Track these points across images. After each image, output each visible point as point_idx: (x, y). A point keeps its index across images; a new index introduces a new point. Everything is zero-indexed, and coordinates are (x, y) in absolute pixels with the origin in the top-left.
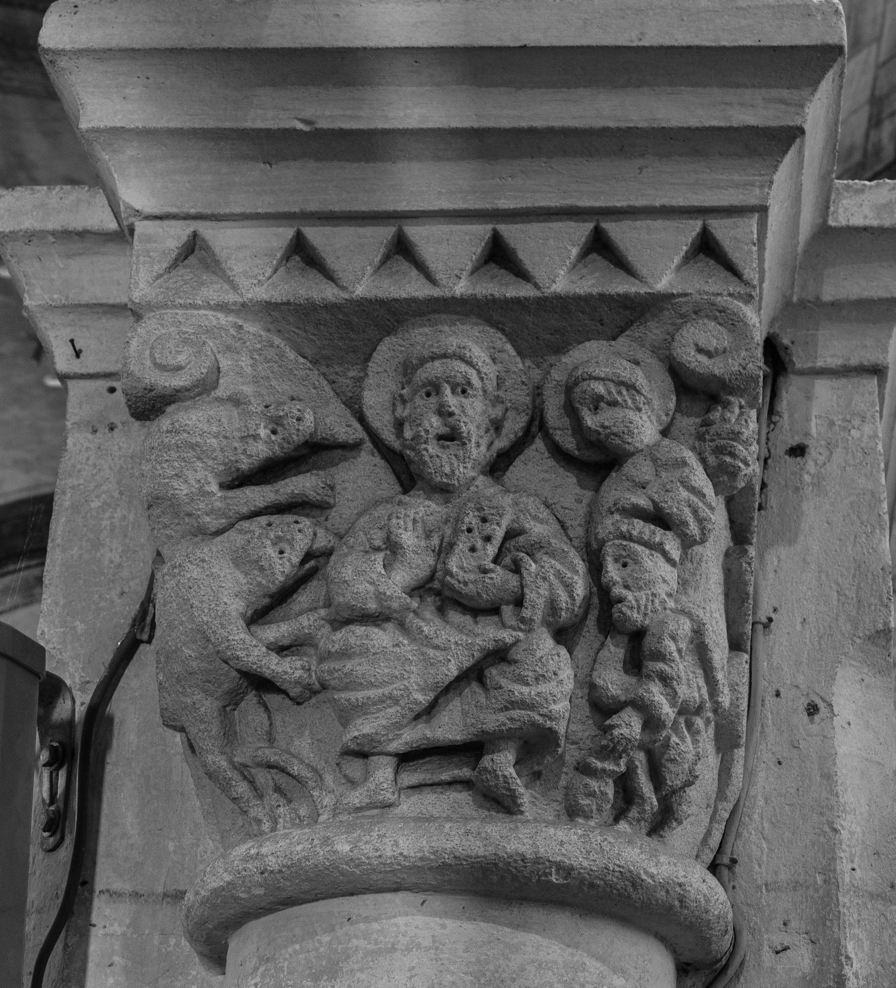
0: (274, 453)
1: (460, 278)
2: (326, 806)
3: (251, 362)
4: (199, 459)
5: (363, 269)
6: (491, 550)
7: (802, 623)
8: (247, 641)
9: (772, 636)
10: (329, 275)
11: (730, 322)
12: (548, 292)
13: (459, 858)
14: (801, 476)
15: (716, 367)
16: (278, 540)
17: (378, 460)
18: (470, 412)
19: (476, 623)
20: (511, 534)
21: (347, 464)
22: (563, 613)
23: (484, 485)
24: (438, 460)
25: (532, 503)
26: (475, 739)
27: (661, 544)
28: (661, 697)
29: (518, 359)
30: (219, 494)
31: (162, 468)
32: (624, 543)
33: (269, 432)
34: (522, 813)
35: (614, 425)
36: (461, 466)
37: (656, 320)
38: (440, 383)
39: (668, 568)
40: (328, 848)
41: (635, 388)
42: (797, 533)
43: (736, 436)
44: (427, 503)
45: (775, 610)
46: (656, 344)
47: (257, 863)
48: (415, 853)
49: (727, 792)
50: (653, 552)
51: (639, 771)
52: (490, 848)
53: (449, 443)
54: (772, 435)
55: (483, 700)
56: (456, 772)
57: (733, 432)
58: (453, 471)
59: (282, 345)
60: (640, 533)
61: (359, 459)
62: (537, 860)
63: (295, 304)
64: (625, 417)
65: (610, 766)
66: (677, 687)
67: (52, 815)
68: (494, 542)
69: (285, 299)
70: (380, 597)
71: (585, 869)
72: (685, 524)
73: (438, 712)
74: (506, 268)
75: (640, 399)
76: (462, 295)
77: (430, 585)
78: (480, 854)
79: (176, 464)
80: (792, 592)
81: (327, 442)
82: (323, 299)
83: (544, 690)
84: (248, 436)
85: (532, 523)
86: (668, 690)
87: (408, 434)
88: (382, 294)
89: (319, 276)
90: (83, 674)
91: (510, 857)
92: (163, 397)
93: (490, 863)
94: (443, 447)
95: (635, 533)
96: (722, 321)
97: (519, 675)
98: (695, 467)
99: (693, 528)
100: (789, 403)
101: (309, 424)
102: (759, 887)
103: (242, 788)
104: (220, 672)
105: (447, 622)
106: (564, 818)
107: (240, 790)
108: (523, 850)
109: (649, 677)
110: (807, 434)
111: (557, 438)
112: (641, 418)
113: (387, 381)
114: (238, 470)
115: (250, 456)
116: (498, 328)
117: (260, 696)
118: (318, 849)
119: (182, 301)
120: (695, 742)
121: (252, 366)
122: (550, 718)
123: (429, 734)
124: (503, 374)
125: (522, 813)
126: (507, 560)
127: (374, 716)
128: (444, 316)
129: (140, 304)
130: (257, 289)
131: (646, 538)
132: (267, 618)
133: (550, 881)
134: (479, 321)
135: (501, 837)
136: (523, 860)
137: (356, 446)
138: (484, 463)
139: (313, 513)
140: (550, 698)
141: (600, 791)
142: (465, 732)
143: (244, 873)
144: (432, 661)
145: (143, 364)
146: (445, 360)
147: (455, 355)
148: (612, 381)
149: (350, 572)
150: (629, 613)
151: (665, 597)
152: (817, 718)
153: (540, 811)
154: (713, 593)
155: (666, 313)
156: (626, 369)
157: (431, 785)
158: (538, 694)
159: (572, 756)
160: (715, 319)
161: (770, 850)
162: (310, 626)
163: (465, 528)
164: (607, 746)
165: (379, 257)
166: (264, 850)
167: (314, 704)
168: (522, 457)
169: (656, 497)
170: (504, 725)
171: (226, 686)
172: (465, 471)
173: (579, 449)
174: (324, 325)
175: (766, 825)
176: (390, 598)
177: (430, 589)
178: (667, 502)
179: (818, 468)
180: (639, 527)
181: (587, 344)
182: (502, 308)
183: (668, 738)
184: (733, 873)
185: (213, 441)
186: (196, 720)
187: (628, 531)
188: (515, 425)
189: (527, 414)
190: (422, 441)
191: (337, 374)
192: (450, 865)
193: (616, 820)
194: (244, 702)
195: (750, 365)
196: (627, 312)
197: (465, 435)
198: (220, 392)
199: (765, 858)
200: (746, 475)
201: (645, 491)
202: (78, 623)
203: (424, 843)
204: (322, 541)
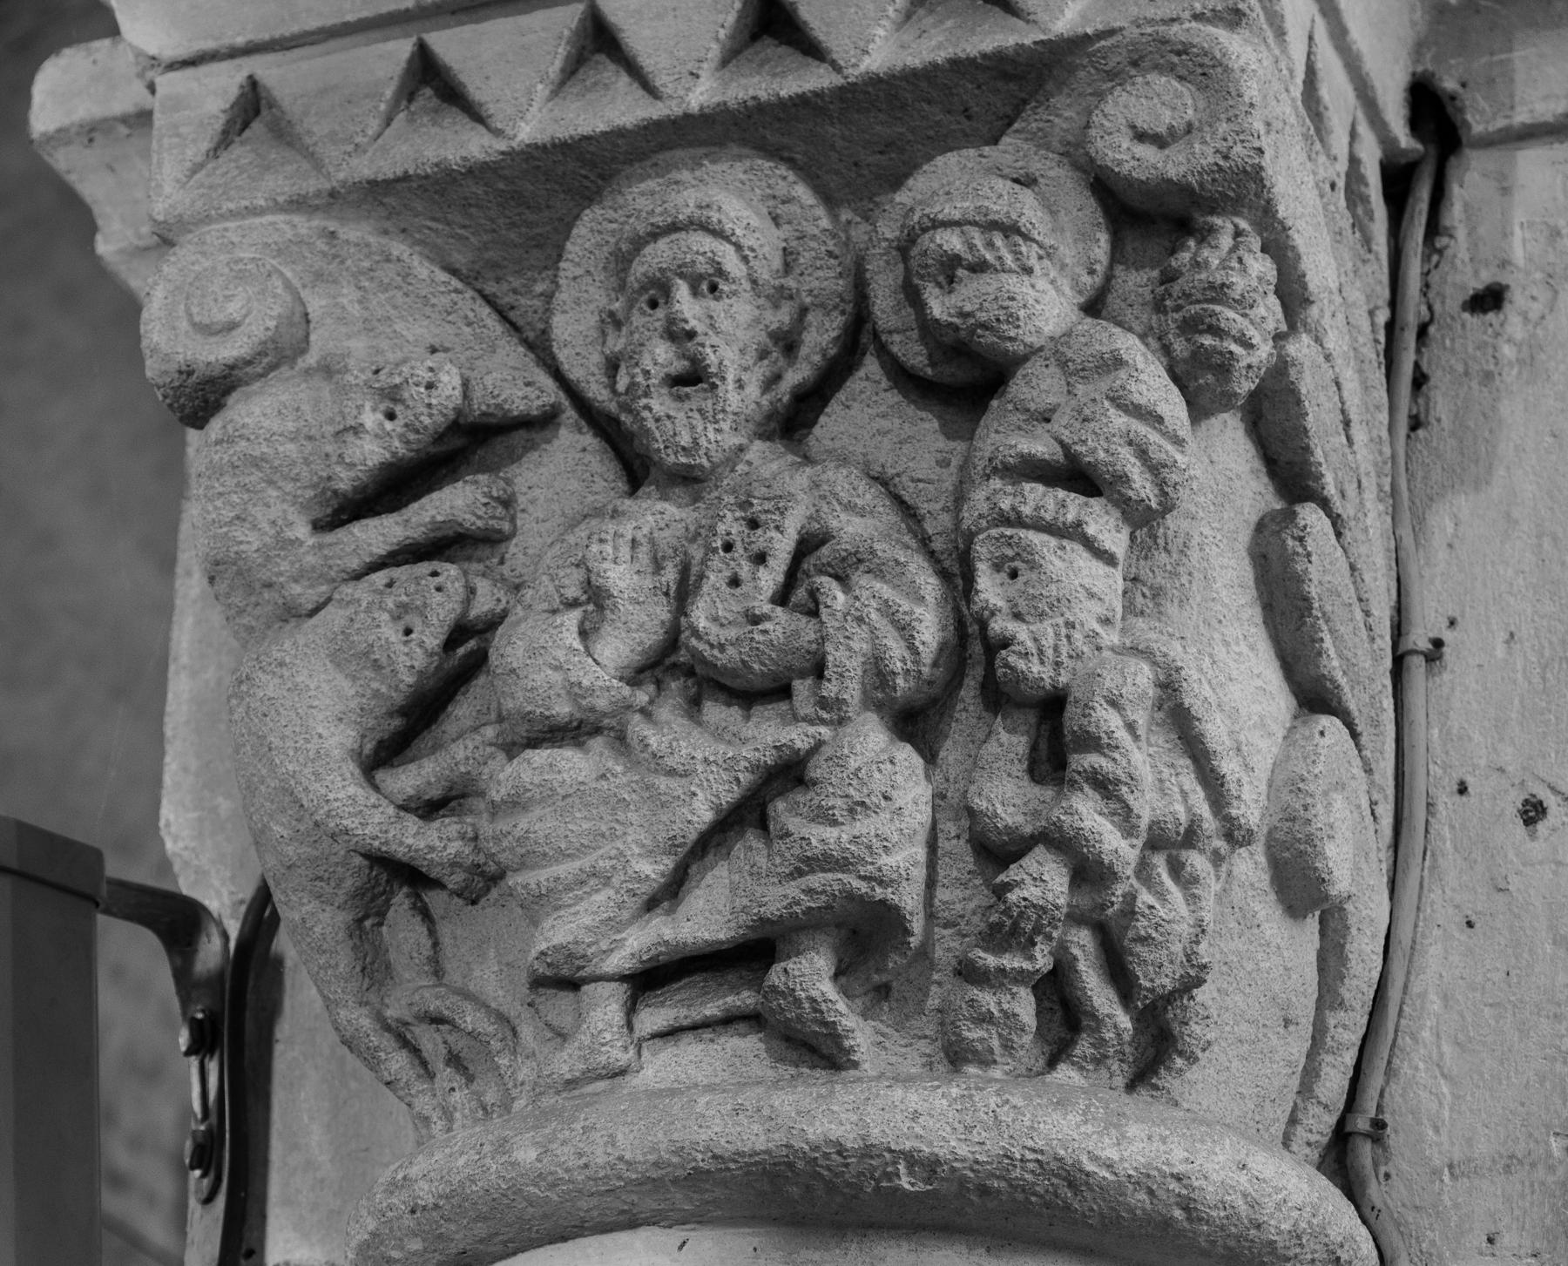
0: (394, 454)
1: (698, 77)
2: (522, 1084)
3: (360, 294)
4: (271, 482)
5: (529, 92)
6: (770, 578)
7: (1507, 642)
8: (361, 800)
9: (1446, 676)
10: (476, 115)
11: (1200, 71)
12: (853, 74)
13: (721, 1157)
14: (1495, 348)
15: (1173, 164)
16: (404, 608)
17: (589, 439)
18: (725, 324)
19: (747, 718)
20: (807, 545)
21: (536, 454)
22: (900, 681)
23: (766, 459)
24: (668, 423)
25: (843, 480)
26: (752, 936)
27: (1079, 524)
28: (1099, 818)
29: (820, 211)
30: (311, 541)
31: (216, 508)
32: (1008, 532)
33: (380, 416)
34: (855, 1065)
35: (981, 309)
36: (710, 428)
37: (1066, 90)
38: (669, 280)
39: (1099, 568)
40: (505, 1158)
41: (1019, 232)
42: (1491, 465)
43: (1219, 292)
44: (660, 506)
45: (1452, 623)
46: (1070, 138)
47: (404, 1195)
48: (644, 1154)
49: (1343, 991)
50: (1065, 542)
51: (1082, 966)
52: (776, 1136)
53: (687, 389)
54: (1435, 278)
55: (762, 861)
56: (729, 999)
57: (1212, 286)
58: (695, 441)
59: (405, 256)
60: (1037, 508)
61: (556, 443)
62: (868, 1151)
63: (418, 176)
64: (1000, 290)
65: (1012, 961)
66: (1130, 799)
67: (200, 1140)
68: (771, 562)
69: (399, 172)
70: (574, 691)
71: (964, 1160)
72: (1124, 479)
73: (689, 892)
74: (789, 43)
75: (1030, 252)
76: (702, 108)
77: (673, 659)
78: (760, 1147)
79: (235, 498)
80: (1485, 585)
81: (493, 420)
82: (464, 159)
83: (865, 831)
84: (346, 430)
85: (843, 517)
86: (1114, 805)
87: (622, 383)
88: (563, 132)
89: (462, 119)
90: (233, 889)
91: (816, 1148)
92: (211, 381)
93: (779, 1164)
94: (679, 398)
95: (1026, 510)
96: (1183, 72)
97: (819, 807)
98: (1140, 366)
99: (1142, 486)
100: (1466, 206)
101: (448, 392)
102: (1436, 1172)
103: (398, 1062)
104: (334, 859)
105: (700, 724)
106: (942, 1068)
107: (394, 1067)
108: (839, 1133)
109: (1073, 783)
110: (1504, 264)
111: (895, 349)
112: (1033, 286)
113: (591, 289)
114: (335, 492)
115: (352, 465)
116: (782, 159)
117: (418, 896)
118: (488, 1161)
119: (232, 206)
120: (1192, 899)
121: (360, 302)
122: (881, 883)
123: (668, 934)
124: (794, 243)
125: (855, 1065)
126: (800, 594)
127: (573, 910)
128: (679, 153)
129: (165, 222)
130: (355, 162)
131: (1048, 517)
132: (409, 753)
133: (898, 1189)
134: (746, 151)
135: (798, 1113)
136: (839, 1153)
137: (546, 421)
138: (758, 418)
139: (479, 553)
140: (876, 843)
141: (1002, 1011)
142: (733, 924)
143: (390, 1214)
144: (663, 798)
145: (174, 328)
146: (674, 236)
147: (692, 223)
148: (975, 223)
149: (520, 653)
150: (1021, 665)
151: (1099, 629)
152: (1541, 827)
153: (893, 1059)
154: (1225, 605)
155: (1082, 74)
156: (1000, 196)
157: (695, 1027)
158: (855, 839)
159: (949, 950)
160: (1172, 68)
161: (1456, 1097)
162: (467, 758)
163: (719, 543)
164: (1000, 925)
165: (558, 64)
166: (414, 1171)
167: (497, 900)
168: (841, 395)
169: (1066, 436)
170: (798, 903)
171: (348, 883)
172: (719, 438)
173: (933, 364)
174: (477, 206)
175: (1447, 1048)
176: (591, 691)
177: (675, 665)
178: (1084, 442)
179: (1530, 327)
180: (1037, 498)
181: (940, 160)
182: (779, 120)
183: (1131, 898)
184: (1385, 1149)
185: (291, 448)
186: (312, 948)
187: (1013, 508)
188: (821, 336)
189: (843, 313)
190: (640, 392)
191: (515, 291)
192: (708, 1171)
193: (1052, 1064)
194: (392, 909)
195: (1238, 149)
196: (1012, 86)
197: (713, 370)
198: (311, 359)
199: (1446, 1114)
200: (1249, 367)
201: (1048, 426)
202: (220, 800)
203: (660, 1135)
204: (483, 605)
